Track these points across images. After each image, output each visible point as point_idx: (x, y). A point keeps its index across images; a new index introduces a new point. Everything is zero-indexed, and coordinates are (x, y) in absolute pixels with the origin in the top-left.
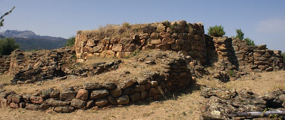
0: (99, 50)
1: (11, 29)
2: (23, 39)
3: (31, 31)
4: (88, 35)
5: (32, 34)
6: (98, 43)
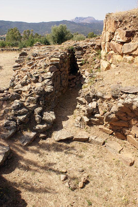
0: (133, 51)
1: (78, 17)
2: (86, 23)
3: (92, 17)
4: (118, 20)
5: (93, 19)
6: (133, 37)
